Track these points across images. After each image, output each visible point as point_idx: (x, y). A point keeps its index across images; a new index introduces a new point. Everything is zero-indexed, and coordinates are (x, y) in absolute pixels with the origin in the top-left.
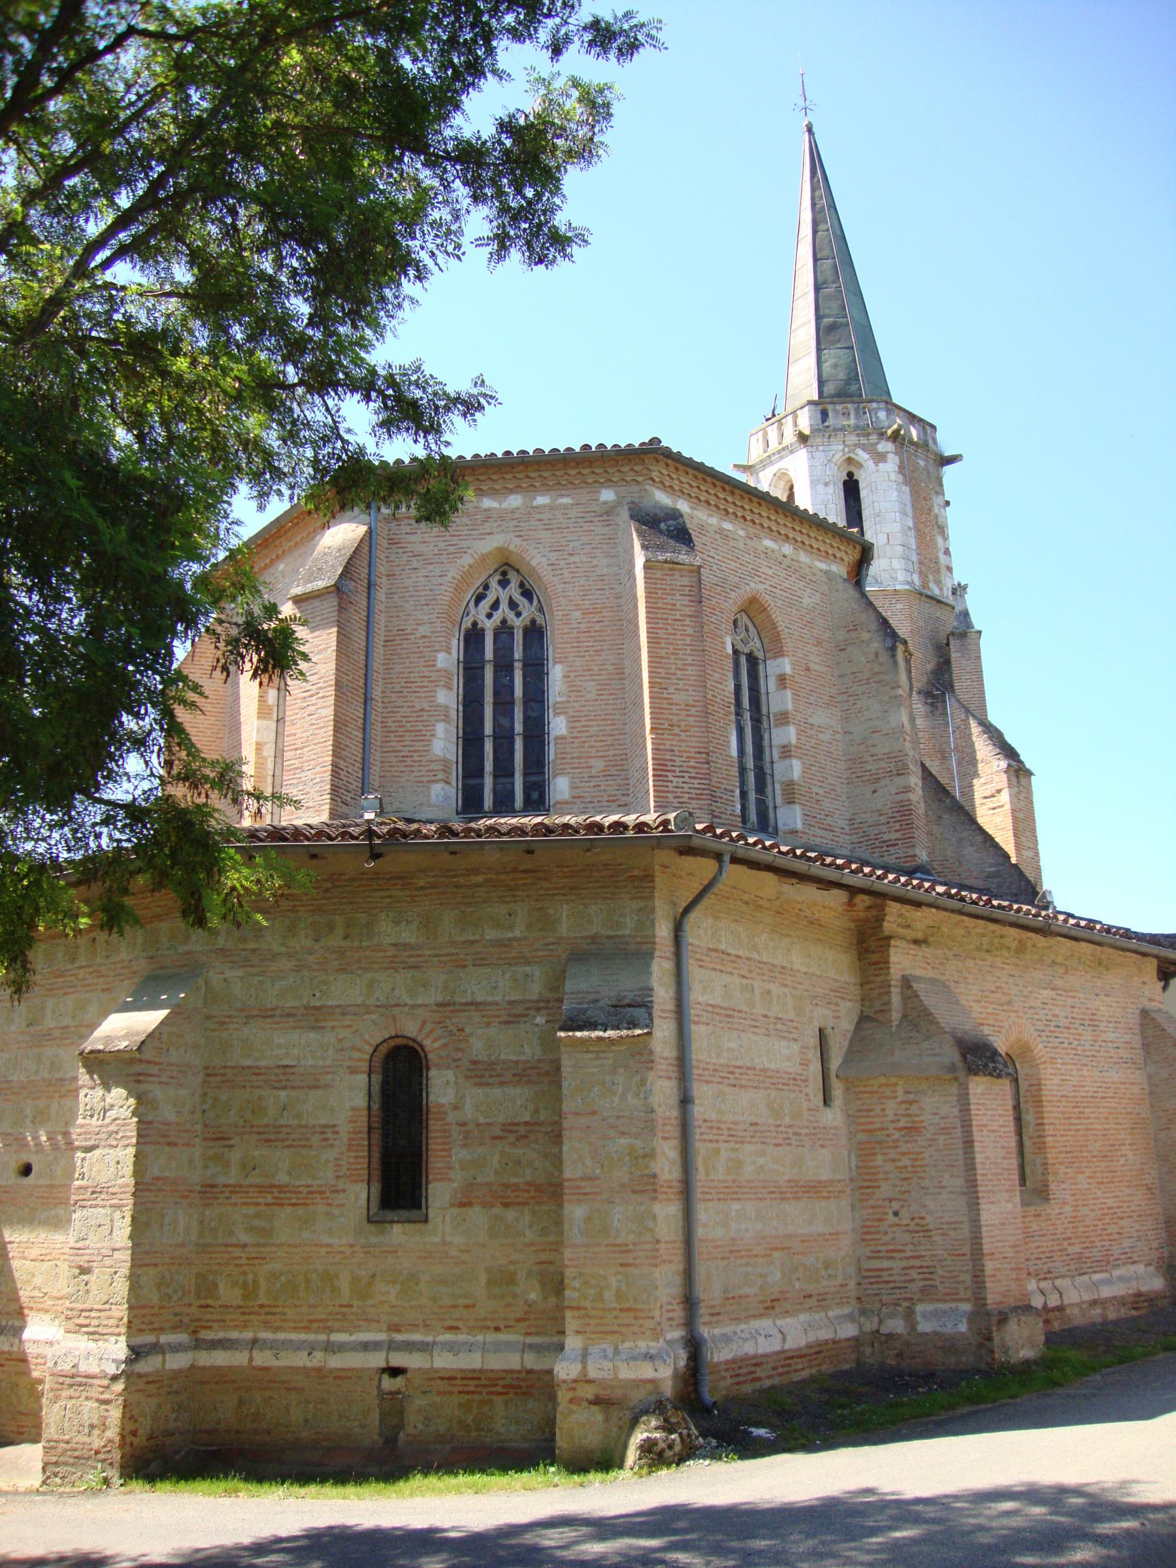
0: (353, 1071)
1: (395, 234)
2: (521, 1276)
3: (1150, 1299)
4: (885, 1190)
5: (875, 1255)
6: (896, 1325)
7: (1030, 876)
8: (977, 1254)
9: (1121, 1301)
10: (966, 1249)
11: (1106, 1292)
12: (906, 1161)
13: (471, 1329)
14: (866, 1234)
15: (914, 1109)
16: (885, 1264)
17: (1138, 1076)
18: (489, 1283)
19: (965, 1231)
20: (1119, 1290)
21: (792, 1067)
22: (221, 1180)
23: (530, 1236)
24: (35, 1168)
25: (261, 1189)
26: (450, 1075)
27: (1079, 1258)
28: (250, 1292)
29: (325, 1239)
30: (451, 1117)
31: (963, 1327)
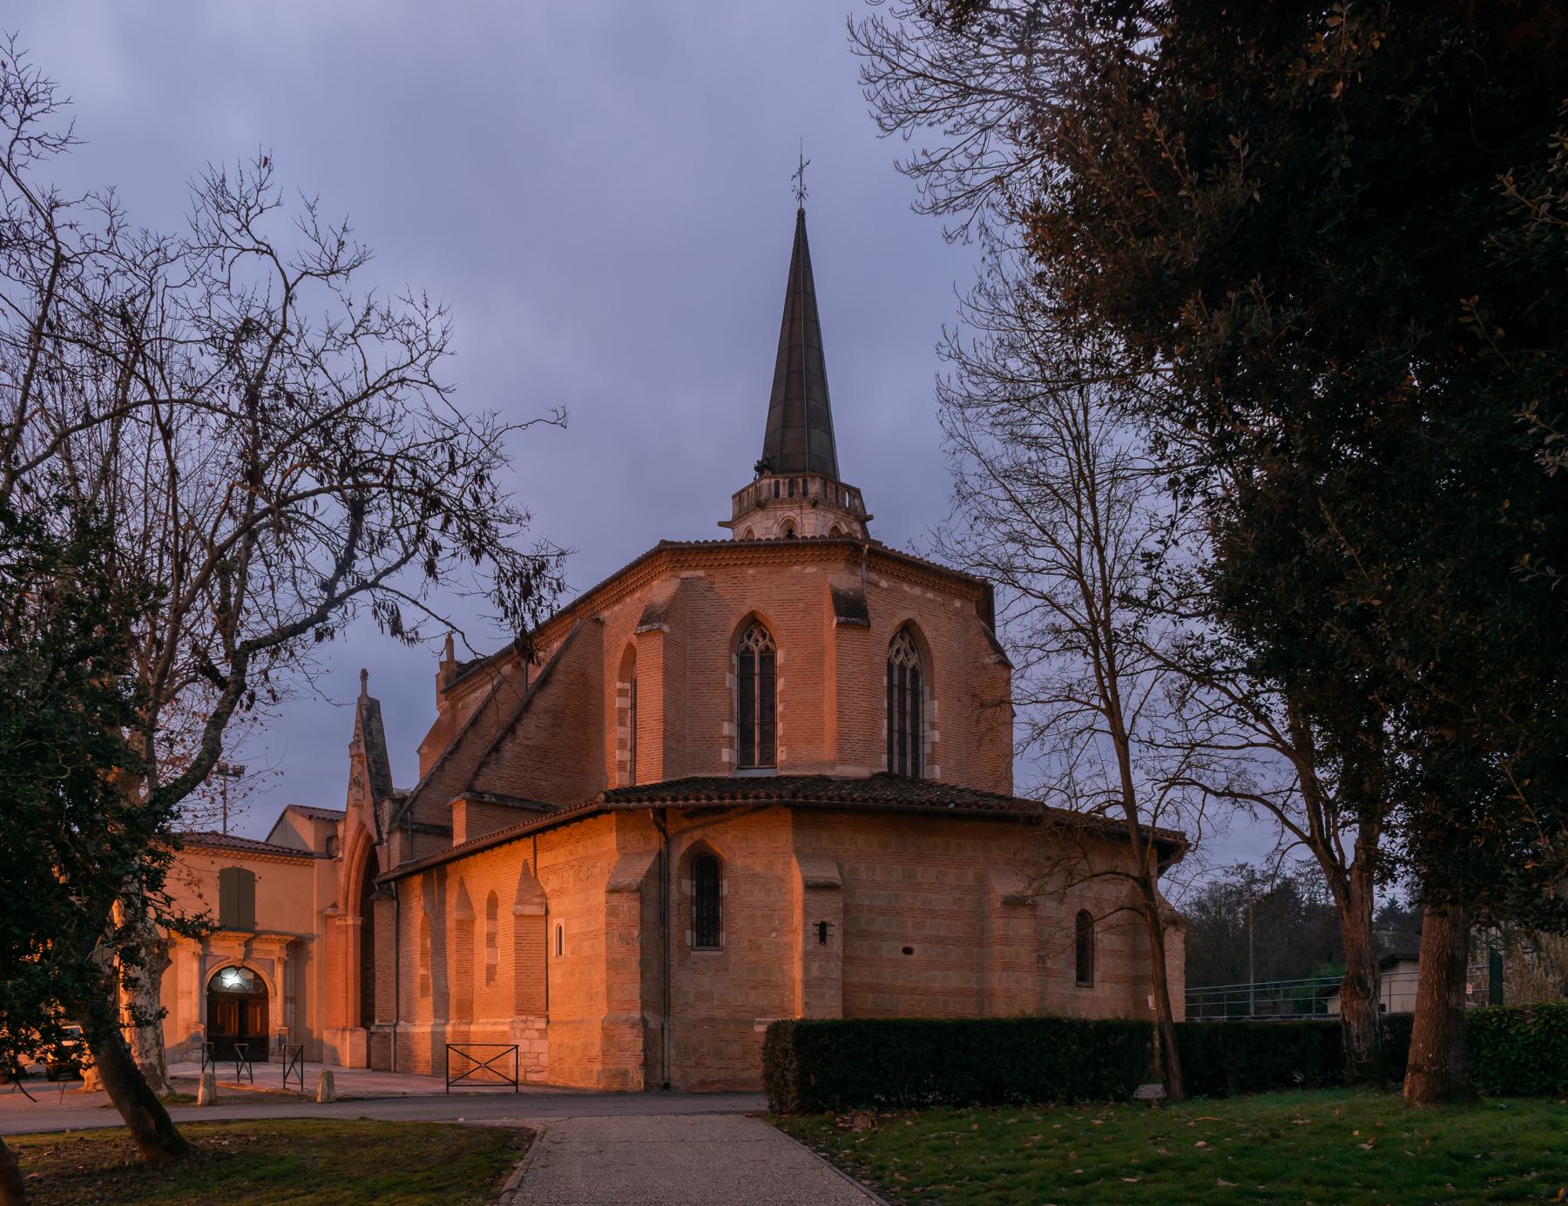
24: (910, 957)
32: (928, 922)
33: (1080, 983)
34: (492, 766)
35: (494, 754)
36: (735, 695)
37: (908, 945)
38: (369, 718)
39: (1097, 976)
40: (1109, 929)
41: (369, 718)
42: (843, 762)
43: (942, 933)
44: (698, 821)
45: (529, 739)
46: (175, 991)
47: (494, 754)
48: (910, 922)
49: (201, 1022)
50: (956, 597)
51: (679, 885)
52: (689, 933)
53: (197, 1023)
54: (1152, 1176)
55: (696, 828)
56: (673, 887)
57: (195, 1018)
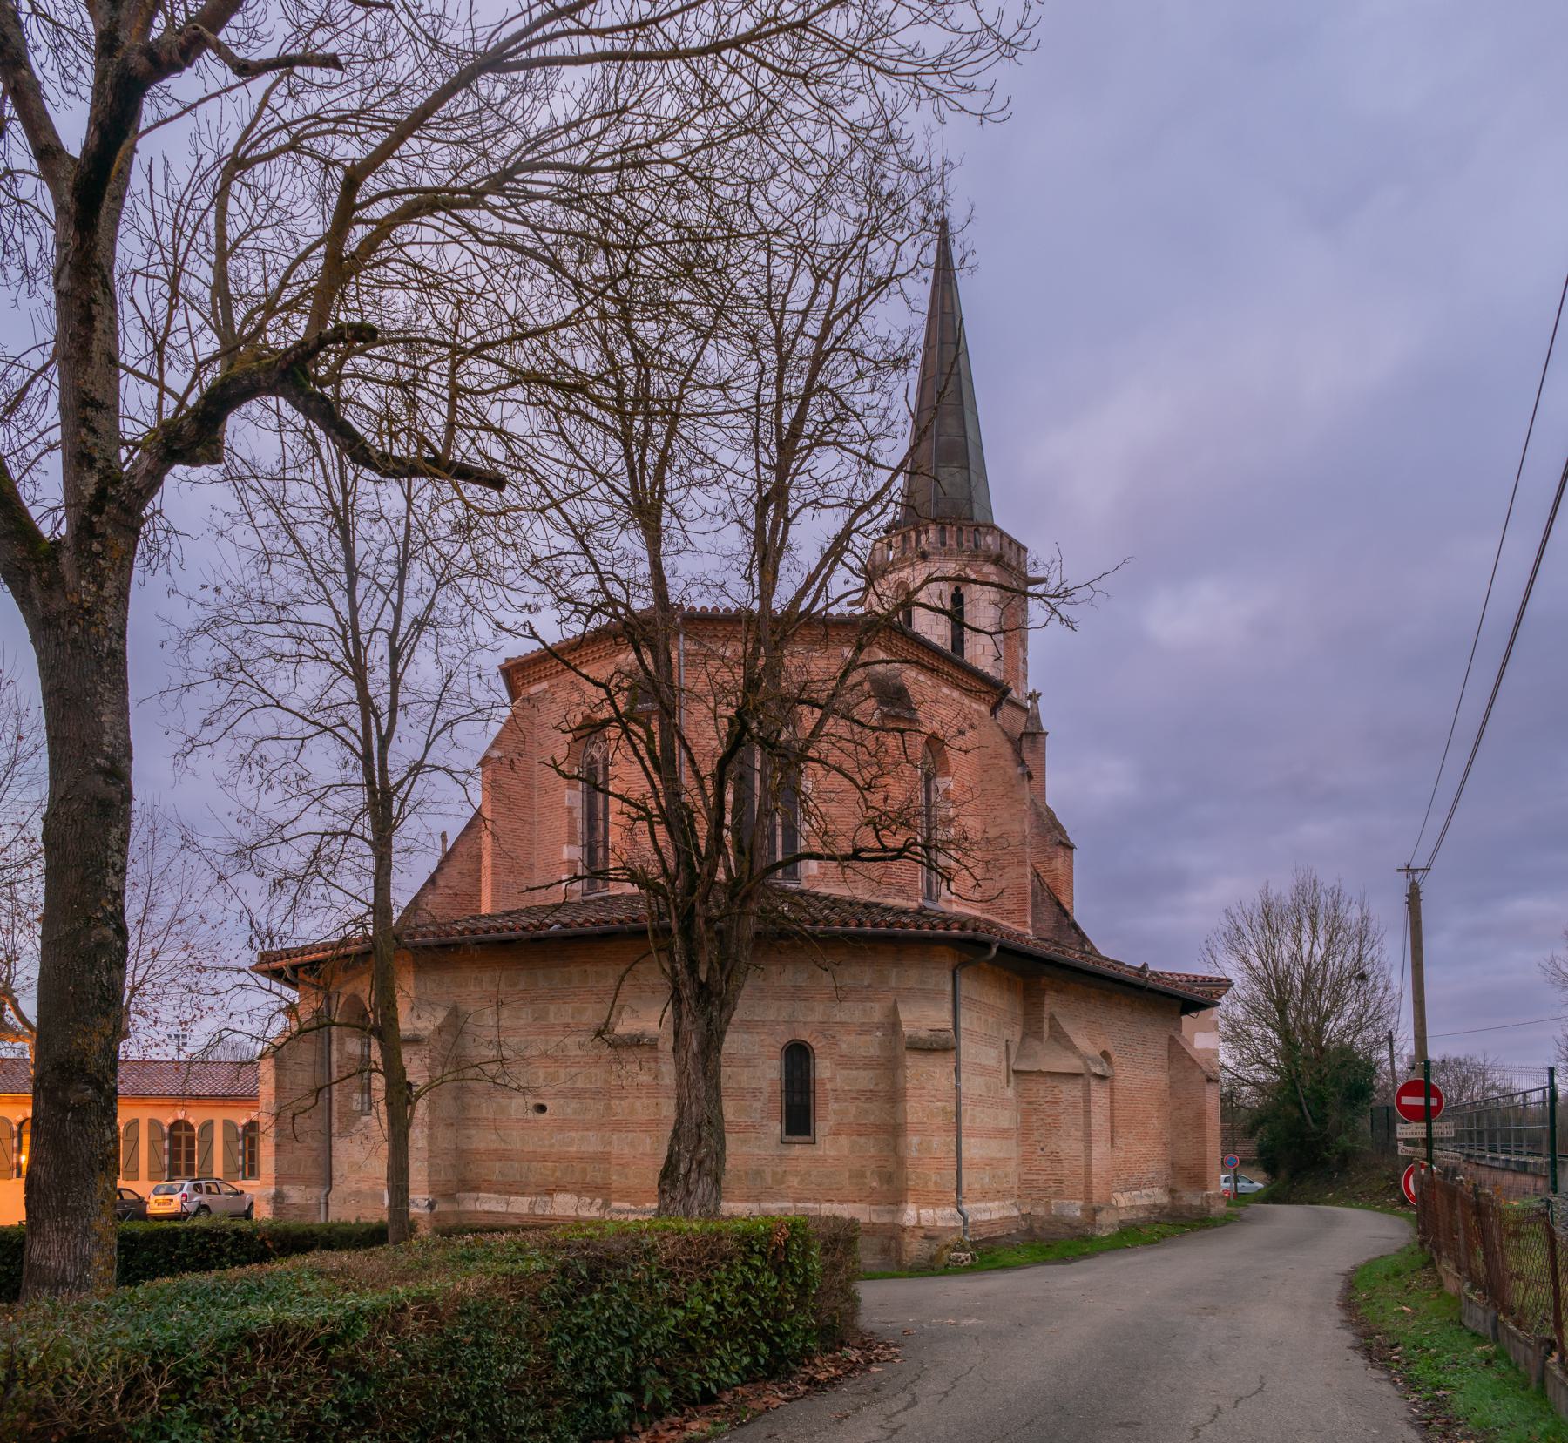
0: (770, 1058)
1: (754, 533)
3: (1162, 1208)
4: (1036, 1136)
5: (1029, 1172)
6: (1040, 1211)
8: (1088, 1173)
9: (1145, 1208)
10: (1082, 1171)
11: (1139, 1202)
12: (1049, 1120)
13: (840, 1202)
14: (1025, 1159)
15: (1056, 1091)
17: (1164, 1076)
19: (1082, 1162)
20: (1146, 1201)
21: (994, 1063)
23: (873, 1151)
24: (542, 1116)
26: (827, 1062)
27: (1126, 1181)
29: (757, 1151)
30: (828, 1086)
31: (1078, 1213)
32: (562, 1072)
33: (787, 1138)
36: (578, 814)
37: (540, 1101)
39: (822, 1127)
40: (845, 1062)
43: (579, 1084)
48: (541, 1073)
50: (843, 644)
56: (334, 1047)
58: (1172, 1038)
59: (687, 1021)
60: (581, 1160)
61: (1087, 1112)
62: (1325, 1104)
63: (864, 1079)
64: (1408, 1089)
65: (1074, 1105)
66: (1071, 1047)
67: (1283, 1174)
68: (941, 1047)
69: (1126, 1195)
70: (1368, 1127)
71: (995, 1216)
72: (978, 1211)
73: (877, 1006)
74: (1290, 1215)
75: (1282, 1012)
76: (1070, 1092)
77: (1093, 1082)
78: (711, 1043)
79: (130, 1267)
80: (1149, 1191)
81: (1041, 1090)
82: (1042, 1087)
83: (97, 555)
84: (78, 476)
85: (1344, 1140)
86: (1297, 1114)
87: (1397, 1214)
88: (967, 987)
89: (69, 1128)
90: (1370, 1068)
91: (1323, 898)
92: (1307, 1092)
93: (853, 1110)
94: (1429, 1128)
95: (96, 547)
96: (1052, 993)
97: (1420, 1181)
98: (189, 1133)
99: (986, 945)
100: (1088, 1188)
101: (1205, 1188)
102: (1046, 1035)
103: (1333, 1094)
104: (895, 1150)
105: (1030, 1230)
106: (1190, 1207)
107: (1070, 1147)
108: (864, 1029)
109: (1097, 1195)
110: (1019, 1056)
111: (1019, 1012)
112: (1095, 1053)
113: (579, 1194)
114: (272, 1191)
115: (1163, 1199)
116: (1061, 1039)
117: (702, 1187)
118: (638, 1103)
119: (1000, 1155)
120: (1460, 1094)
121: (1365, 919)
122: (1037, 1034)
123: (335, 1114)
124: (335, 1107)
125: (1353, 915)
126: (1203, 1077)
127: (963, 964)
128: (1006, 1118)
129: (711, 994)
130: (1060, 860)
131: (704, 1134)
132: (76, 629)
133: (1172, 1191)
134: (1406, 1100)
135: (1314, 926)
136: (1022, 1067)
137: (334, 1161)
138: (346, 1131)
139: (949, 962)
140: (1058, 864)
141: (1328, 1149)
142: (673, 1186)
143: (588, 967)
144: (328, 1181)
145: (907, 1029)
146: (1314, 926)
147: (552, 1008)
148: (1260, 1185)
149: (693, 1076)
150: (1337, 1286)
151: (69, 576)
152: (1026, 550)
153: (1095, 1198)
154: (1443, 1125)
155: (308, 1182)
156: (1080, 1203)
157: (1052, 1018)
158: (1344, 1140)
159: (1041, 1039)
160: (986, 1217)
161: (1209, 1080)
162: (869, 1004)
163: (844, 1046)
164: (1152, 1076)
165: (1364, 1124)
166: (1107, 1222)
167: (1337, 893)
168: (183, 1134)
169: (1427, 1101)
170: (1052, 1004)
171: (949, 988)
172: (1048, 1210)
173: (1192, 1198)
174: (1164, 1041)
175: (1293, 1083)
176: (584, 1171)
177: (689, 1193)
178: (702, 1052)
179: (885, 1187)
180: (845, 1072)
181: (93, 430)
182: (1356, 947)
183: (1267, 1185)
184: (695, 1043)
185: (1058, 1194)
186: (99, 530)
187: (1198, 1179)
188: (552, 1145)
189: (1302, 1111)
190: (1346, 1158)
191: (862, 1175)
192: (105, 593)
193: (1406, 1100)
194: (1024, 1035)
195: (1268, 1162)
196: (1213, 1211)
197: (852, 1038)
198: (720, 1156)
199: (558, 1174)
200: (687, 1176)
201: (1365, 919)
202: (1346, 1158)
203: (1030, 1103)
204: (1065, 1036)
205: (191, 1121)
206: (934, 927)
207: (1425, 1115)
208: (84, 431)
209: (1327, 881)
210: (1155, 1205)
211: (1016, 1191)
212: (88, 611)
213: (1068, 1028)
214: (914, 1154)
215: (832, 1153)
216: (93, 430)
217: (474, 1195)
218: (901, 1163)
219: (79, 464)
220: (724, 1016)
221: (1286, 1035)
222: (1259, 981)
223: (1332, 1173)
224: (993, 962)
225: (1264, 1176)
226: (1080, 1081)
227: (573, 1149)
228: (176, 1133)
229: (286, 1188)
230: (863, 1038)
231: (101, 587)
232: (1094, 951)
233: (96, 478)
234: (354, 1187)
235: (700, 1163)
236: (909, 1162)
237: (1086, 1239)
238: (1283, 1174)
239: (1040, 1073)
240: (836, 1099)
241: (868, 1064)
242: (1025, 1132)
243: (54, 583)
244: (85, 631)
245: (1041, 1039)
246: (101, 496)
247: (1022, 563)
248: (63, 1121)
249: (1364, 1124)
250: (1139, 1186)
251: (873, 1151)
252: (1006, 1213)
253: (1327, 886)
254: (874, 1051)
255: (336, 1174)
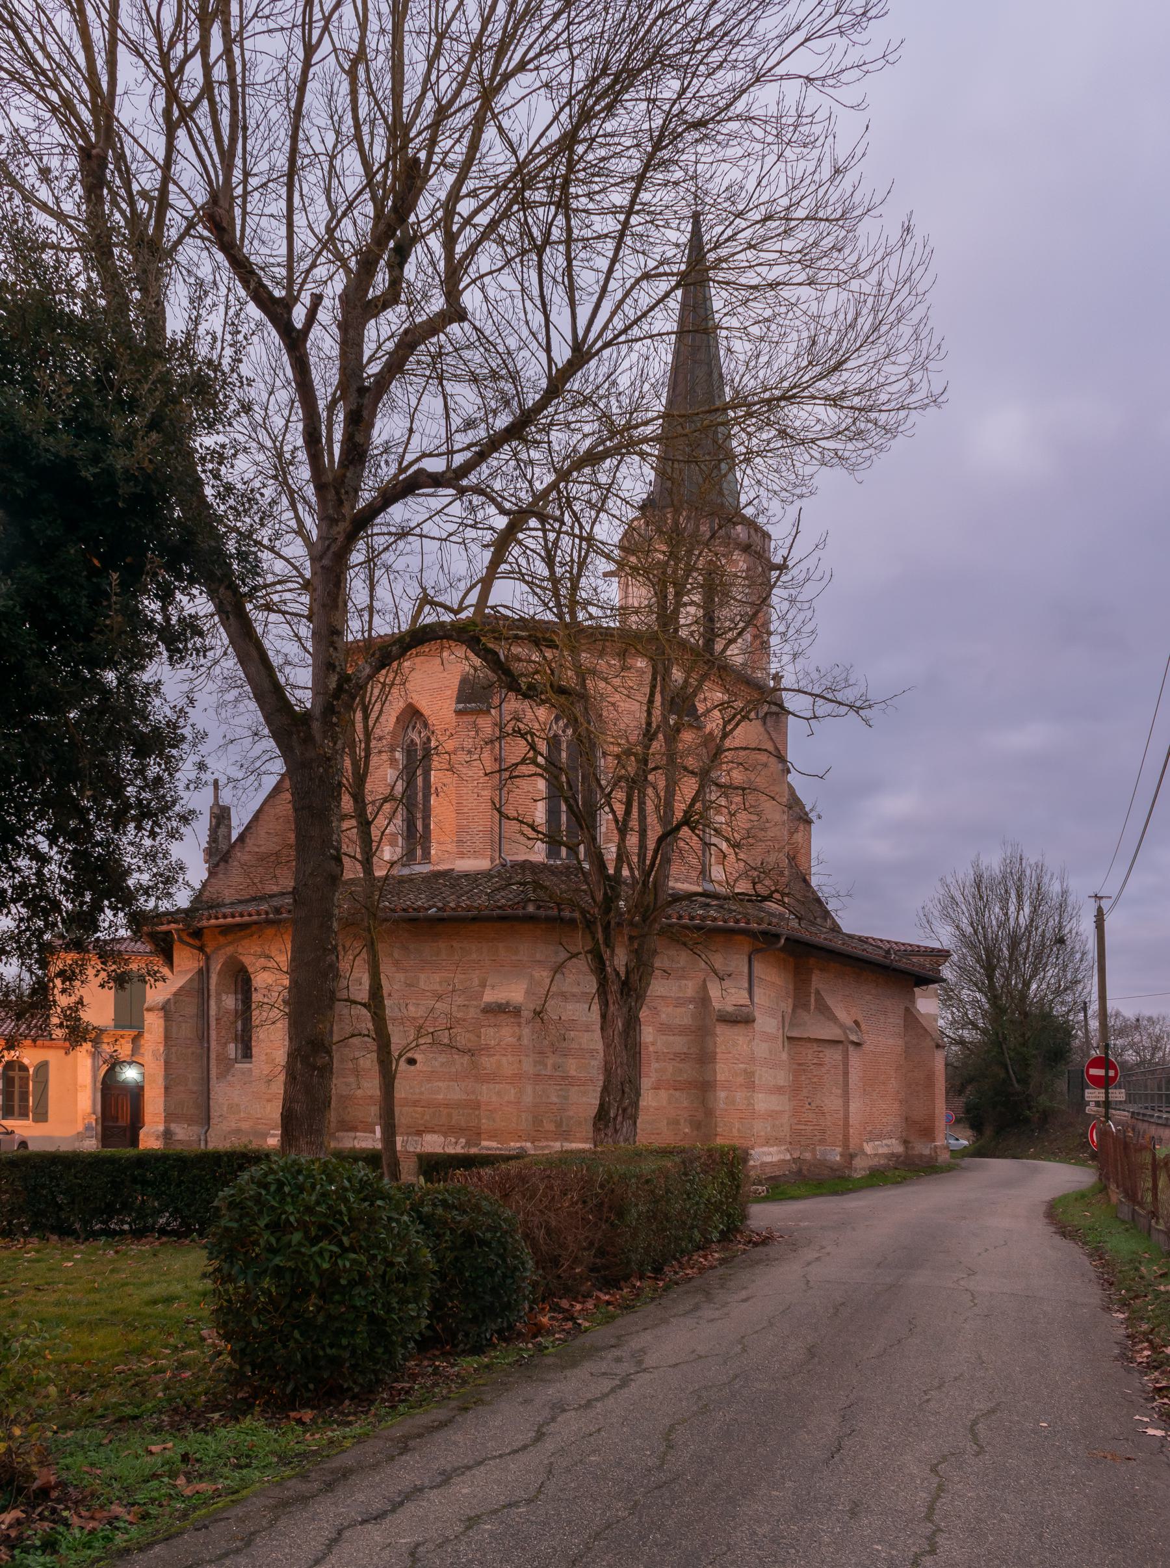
2: (682, 1121)
4: (805, 1093)
6: (808, 1156)
7: (285, 804)
8: (846, 1125)
10: (841, 1123)
11: (880, 1151)
15: (821, 1055)
16: (803, 1127)
17: (900, 1042)
18: (668, 1124)
20: (885, 1150)
21: (774, 1031)
22: (543, 1072)
23: (685, 1104)
24: (412, 1068)
25: (563, 1078)
26: (650, 1029)
28: (559, 1125)
30: (651, 1049)
31: (838, 1158)
34: (221, 876)
35: (222, 864)
38: (218, 826)
41: (218, 826)
42: (462, 855)
44: (230, 938)
45: (259, 846)
46: (76, 1084)
47: (222, 864)
49: (94, 1113)
51: (219, 1001)
52: (232, 1046)
53: (89, 1114)
54: (70, 1287)
55: (230, 943)
56: (213, 1003)
57: (89, 1109)
58: (907, 1009)
59: (612, 1008)
60: (447, 1106)
61: (846, 1074)
62: (1027, 1065)
63: (679, 1043)
64: (1097, 1063)
65: (835, 1067)
66: (834, 1019)
67: (988, 1132)
68: (741, 1019)
69: (871, 1144)
70: (1065, 1087)
71: (775, 1159)
72: (765, 1154)
73: (690, 984)
74: (1000, 1166)
75: (990, 977)
76: (832, 1056)
77: (851, 1048)
78: (632, 1024)
79: (183, 1182)
80: (888, 1142)
81: (809, 1054)
82: (810, 1051)
83: (335, 724)
84: (326, 677)
85: (1043, 1099)
86: (1003, 1075)
87: (1089, 1166)
88: (759, 968)
89: (315, 1080)
90: (1066, 1031)
91: (1028, 873)
92: (1012, 1054)
93: (670, 1069)
94: (1107, 1093)
95: (335, 720)
96: (817, 972)
97: (1100, 1135)
98: (22, 1074)
99: (777, 936)
100: (846, 1138)
101: (934, 1140)
102: (812, 1007)
103: (1034, 1056)
104: (704, 1102)
105: (800, 1171)
106: (921, 1156)
107: (832, 1103)
108: (680, 1003)
109: (853, 1142)
110: (792, 1025)
111: (791, 987)
112: (849, 1022)
113: (445, 1135)
114: (161, 1128)
115: (899, 1149)
116: (824, 1010)
117: (626, 1128)
118: (504, 1059)
119: (778, 1108)
120: (1153, 1055)
121: (1064, 893)
122: (806, 1007)
123: (213, 1062)
124: (213, 1055)
125: (1055, 888)
126: (933, 1044)
127: (758, 951)
128: (782, 1078)
129: (630, 990)
130: (800, 834)
131: (627, 1090)
132: (321, 770)
133: (906, 1142)
134: (1093, 1072)
135: (1019, 897)
136: (795, 1034)
137: (212, 1103)
138: (222, 1076)
139: (747, 948)
140: (799, 837)
141: (1030, 1108)
142: (606, 1126)
143: (455, 944)
144: (207, 1120)
145: (716, 1005)
146: (1019, 897)
147: (422, 976)
148: (966, 1143)
149: (618, 1048)
150: (1043, 1208)
151: (318, 737)
152: (769, 537)
153: (851, 1146)
154: (1117, 1091)
155: (190, 1121)
156: (839, 1149)
157: (818, 992)
158: (1043, 1099)
159: (808, 1011)
160: (768, 1159)
161: (938, 1046)
162: (684, 982)
163: (663, 1016)
164: (891, 1041)
165: (1062, 1085)
166: (861, 1166)
167: (1040, 868)
168: (16, 1074)
169: (1107, 1073)
170: (817, 981)
171: (746, 970)
172: (814, 1154)
173: (923, 1149)
174: (902, 1012)
175: (1000, 1045)
176: (450, 1115)
177: (616, 1131)
178: (624, 1031)
179: (695, 1132)
180: (664, 1037)
181: (335, 649)
182: (1057, 919)
183: (974, 1142)
184: (620, 1024)
185: (822, 1142)
186: (337, 709)
187: (927, 1132)
188: (421, 1093)
189: (1008, 1072)
190: (1046, 1116)
191: (677, 1123)
192: (337, 747)
193: (1093, 1072)
194: (795, 1007)
195: (973, 1118)
196: (940, 1159)
197: (670, 1009)
198: (635, 1105)
199: (427, 1117)
200: (615, 1118)
201: (1064, 893)
202: (1046, 1116)
203: (800, 1064)
204: (828, 1008)
205: (26, 1061)
206: (737, 921)
207: (1103, 1083)
208: (331, 649)
209: (1031, 858)
210: (893, 1154)
211: (788, 1139)
212: (329, 759)
213: (830, 1002)
214: (722, 1106)
215: (654, 1104)
216: (335, 649)
217: (352, 1134)
218: (709, 1113)
219: (328, 669)
220: (638, 1005)
221: (994, 999)
222: (972, 946)
223: (1033, 1131)
224: (782, 949)
225: (969, 1133)
226: (841, 1047)
227: (441, 1097)
228: (11, 1073)
229: (173, 1126)
230: (679, 1010)
231: (335, 744)
232: (836, 929)
233: (336, 678)
234: (234, 1125)
235: (624, 1110)
236: (718, 1113)
237: (847, 1179)
238: (988, 1132)
239: (809, 1040)
240: (657, 1060)
241: (683, 1031)
242: (795, 1090)
243: (308, 740)
244: (326, 771)
245: (808, 1011)
246: (340, 689)
247: (765, 549)
248: (312, 1076)
249: (1062, 1085)
250: (880, 1137)
251: (685, 1104)
252: (782, 1157)
253: (1032, 861)
254: (687, 1021)
255: (213, 1114)
